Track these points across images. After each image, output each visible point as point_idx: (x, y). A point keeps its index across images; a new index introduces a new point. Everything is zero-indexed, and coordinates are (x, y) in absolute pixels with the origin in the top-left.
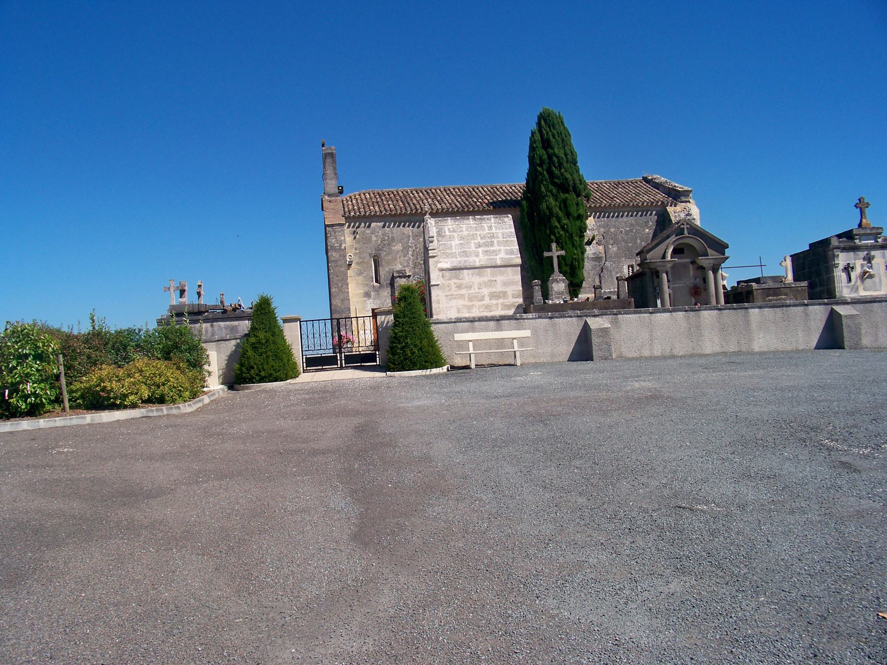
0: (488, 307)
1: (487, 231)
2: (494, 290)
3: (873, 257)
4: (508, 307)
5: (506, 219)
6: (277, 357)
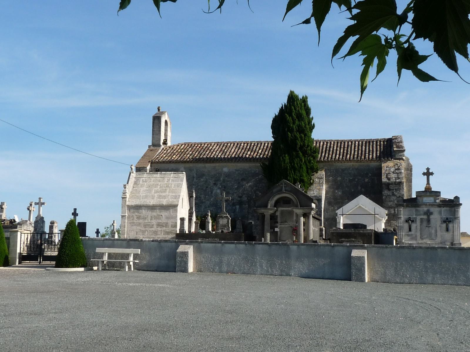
0: (156, 233)
1: (166, 182)
2: (160, 221)
3: (431, 213)
4: (168, 233)
5: (181, 175)
6: (190, 194)
